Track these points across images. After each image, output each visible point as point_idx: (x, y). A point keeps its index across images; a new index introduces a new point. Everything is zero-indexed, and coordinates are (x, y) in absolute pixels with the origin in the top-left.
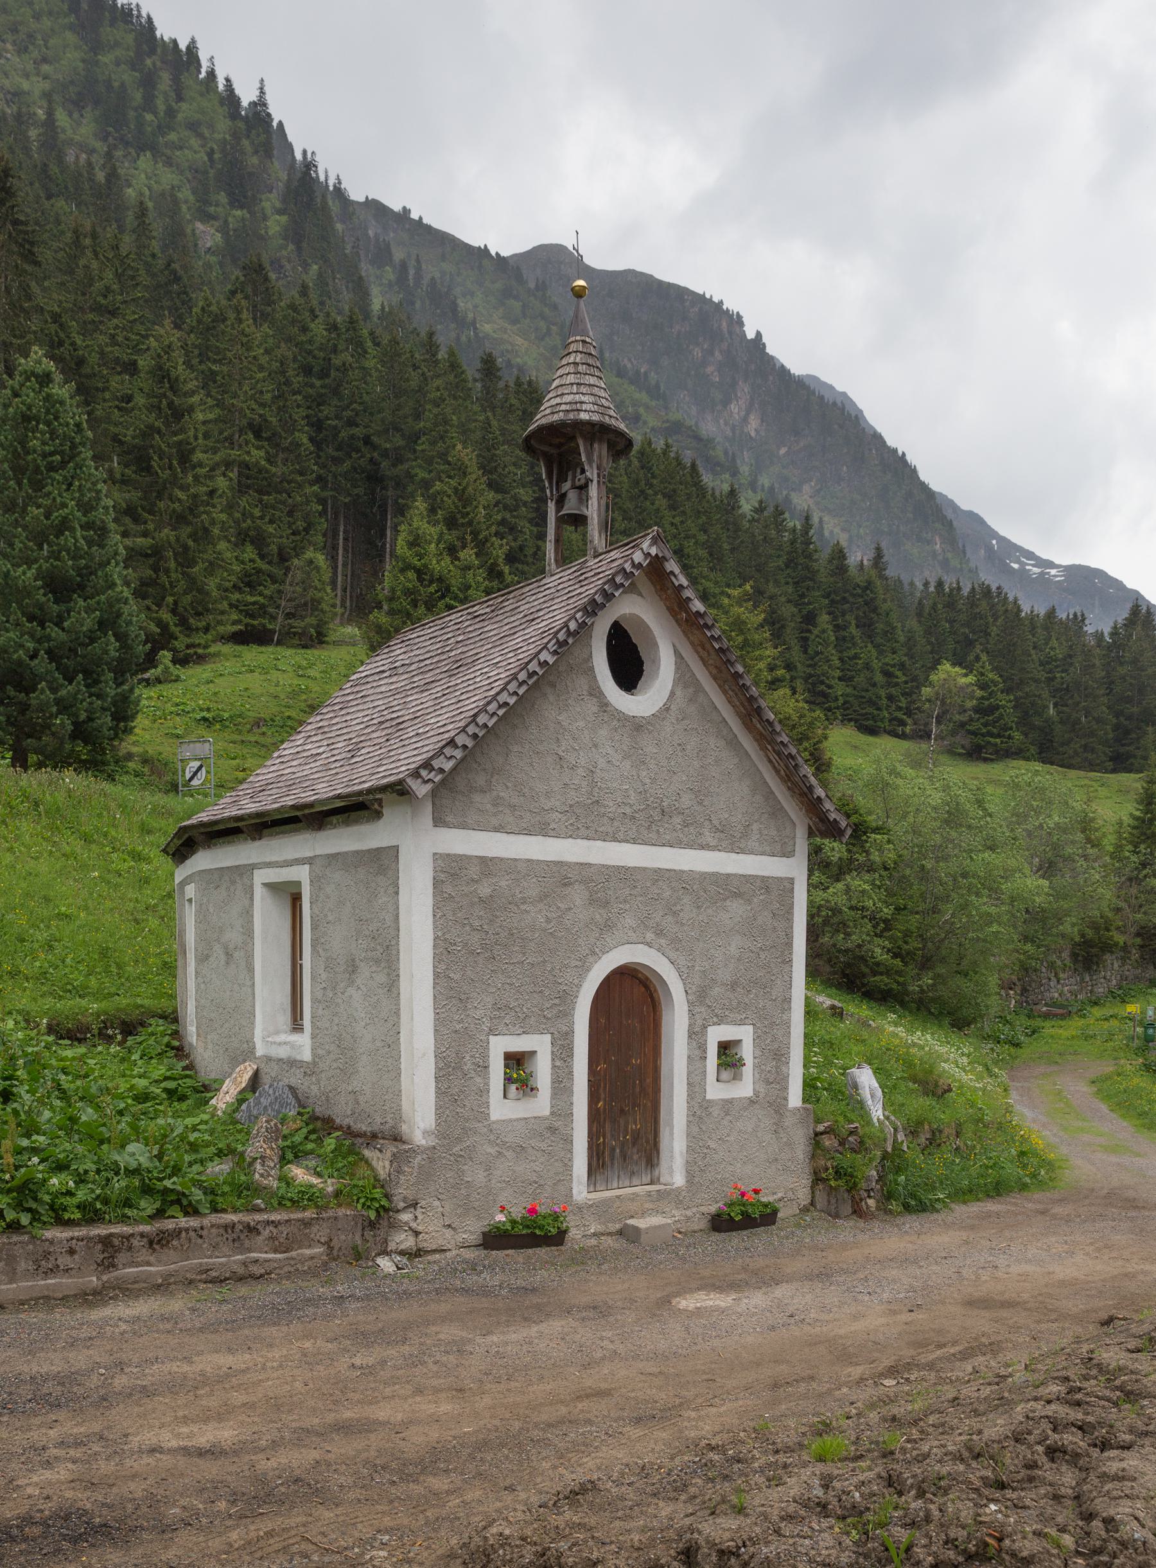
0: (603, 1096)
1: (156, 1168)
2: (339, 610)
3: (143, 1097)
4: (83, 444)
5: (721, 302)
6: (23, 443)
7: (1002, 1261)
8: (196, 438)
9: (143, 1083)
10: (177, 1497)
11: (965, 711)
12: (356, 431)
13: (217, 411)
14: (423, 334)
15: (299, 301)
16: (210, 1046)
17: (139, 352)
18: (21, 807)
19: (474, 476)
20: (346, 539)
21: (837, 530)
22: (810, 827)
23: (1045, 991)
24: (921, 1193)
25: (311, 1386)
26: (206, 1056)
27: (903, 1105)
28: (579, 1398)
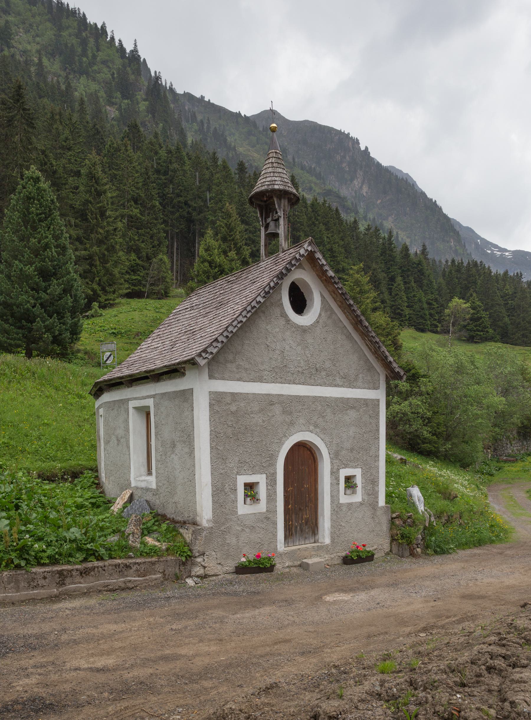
0: (291, 502)
1: (83, 539)
2: (175, 281)
3: (80, 507)
4: (55, 209)
5: (349, 134)
6: (28, 210)
7: (479, 577)
8: (108, 204)
9: (80, 500)
10: (85, 691)
11: (465, 320)
12: (181, 199)
13: (117, 192)
14: (211, 154)
15: (154, 140)
16: (111, 483)
17: (82, 167)
18: (27, 375)
19: (234, 218)
20: (177, 249)
21: (405, 238)
22: (386, 375)
23: (505, 450)
24: (442, 545)
25: (152, 639)
26: (109, 487)
27: (434, 504)
28: (276, 643)
